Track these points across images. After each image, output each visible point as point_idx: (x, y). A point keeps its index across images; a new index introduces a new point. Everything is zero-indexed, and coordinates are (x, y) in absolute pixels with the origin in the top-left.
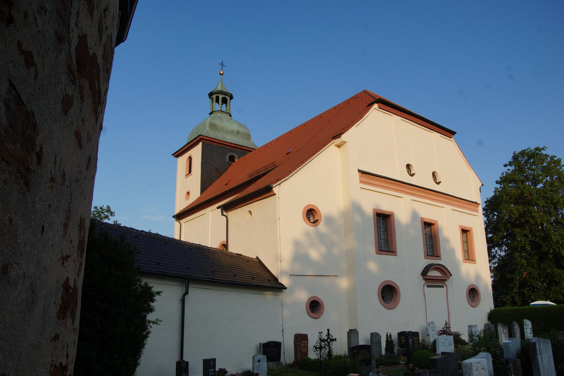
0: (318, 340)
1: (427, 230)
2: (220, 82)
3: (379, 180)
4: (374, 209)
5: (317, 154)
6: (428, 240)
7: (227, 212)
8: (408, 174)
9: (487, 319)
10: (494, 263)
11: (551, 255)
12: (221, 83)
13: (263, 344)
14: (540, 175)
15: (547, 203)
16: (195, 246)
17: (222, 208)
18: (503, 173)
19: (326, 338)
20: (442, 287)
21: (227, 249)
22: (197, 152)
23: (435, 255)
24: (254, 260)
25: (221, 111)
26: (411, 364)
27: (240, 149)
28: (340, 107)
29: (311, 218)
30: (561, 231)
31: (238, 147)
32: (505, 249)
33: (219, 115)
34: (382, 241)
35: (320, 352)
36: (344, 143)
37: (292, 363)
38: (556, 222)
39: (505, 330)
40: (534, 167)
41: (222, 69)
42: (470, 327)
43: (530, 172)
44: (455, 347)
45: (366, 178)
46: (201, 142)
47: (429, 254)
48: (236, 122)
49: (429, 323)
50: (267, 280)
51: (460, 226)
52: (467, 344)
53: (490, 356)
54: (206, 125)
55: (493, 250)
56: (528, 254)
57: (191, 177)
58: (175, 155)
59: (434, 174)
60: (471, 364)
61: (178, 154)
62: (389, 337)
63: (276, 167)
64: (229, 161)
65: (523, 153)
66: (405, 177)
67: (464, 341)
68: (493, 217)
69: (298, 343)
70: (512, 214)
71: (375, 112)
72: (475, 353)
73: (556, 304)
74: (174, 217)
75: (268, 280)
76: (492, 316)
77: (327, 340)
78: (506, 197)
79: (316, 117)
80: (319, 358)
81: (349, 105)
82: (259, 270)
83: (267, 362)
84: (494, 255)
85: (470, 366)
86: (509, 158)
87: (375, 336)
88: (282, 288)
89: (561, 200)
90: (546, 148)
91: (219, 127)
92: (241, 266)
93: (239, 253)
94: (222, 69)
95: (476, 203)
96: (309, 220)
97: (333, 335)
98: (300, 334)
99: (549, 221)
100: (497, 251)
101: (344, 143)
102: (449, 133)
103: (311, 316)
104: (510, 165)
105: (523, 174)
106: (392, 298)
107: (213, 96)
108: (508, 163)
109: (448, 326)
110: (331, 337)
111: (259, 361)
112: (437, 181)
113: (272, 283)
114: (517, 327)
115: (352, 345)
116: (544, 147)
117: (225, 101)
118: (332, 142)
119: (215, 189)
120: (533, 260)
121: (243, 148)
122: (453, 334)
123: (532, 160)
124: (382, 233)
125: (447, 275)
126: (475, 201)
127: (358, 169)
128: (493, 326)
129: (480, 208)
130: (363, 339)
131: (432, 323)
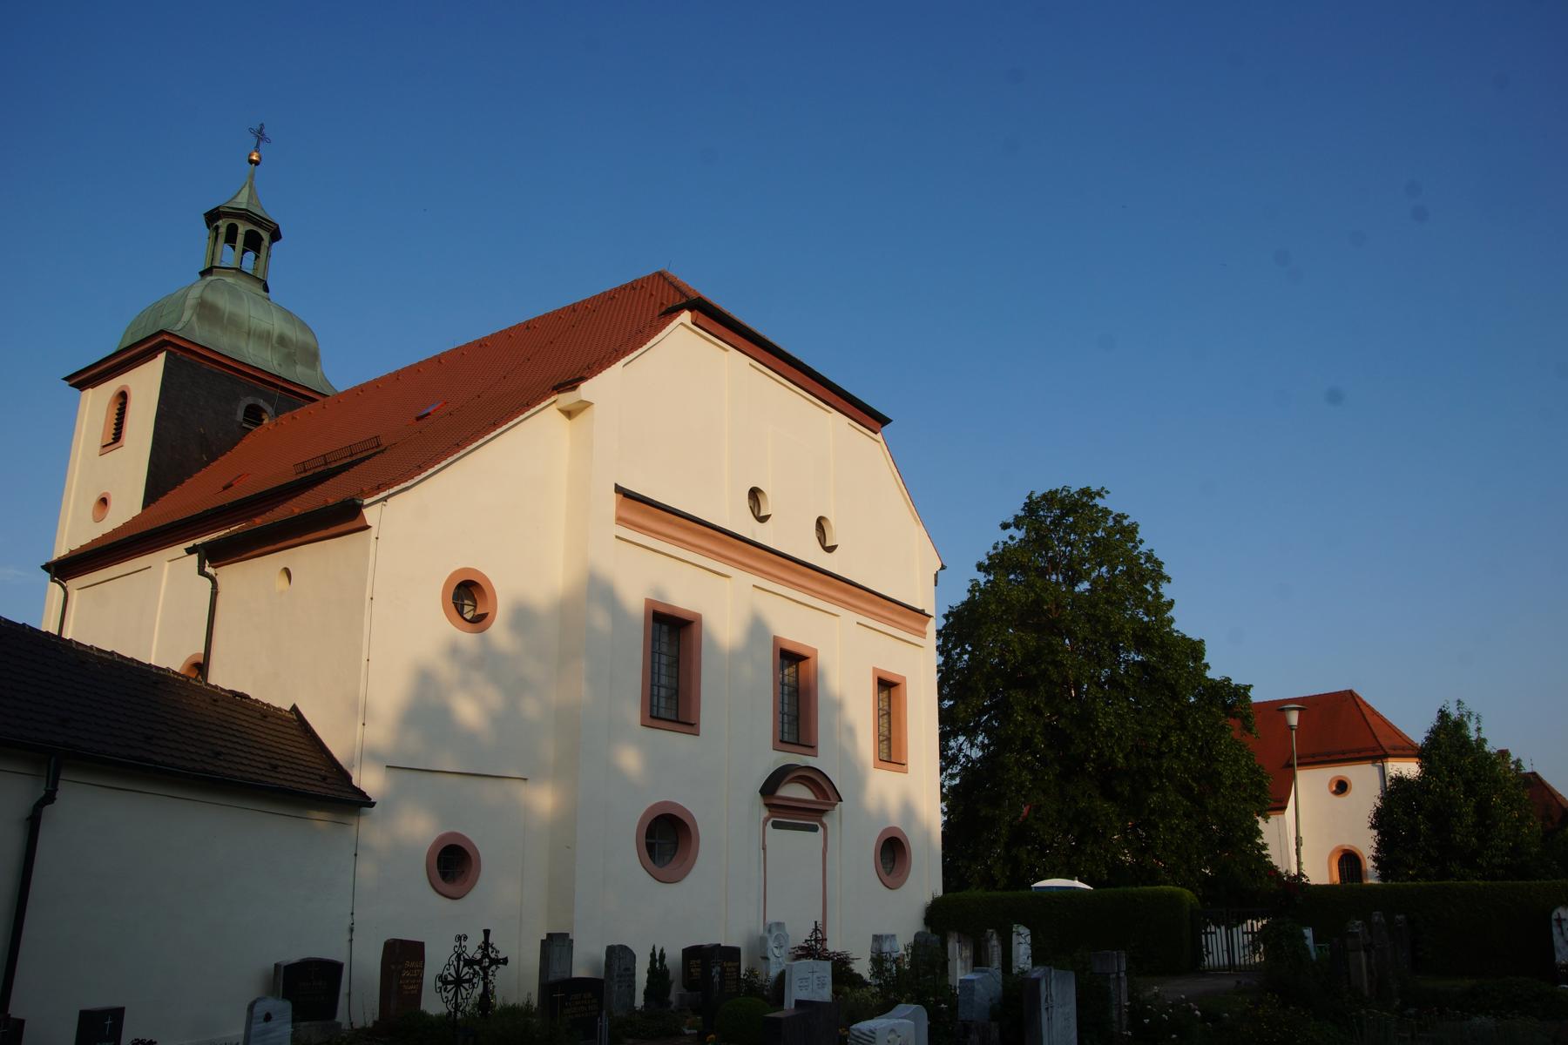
0: (453, 958)
1: (786, 672)
2: (247, 185)
3: (670, 523)
4: (646, 599)
5: (505, 427)
6: (786, 701)
7: (215, 567)
8: (751, 515)
9: (923, 922)
10: (952, 777)
11: (1092, 764)
12: (250, 187)
13: (285, 967)
14: (1087, 560)
15: (1095, 632)
16: (98, 657)
17: (203, 552)
18: (998, 543)
19: (478, 956)
20: (814, 829)
21: (205, 676)
22: (146, 382)
23: (683, 720)
24: (284, 716)
25: (239, 270)
26: (712, 1036)
27: (283, 389)
28: (587, 307)
29: (467, 609)
30: (1120, 706)
31: (276, 382)
32: (982, 742)
33: (230, 280)
34: (663, 692)
35: (456, 993)
36: (585, 405)
37: (370, 1024)
38: (1111, 681)
39: (966, 949)
40: (1072, 537)
41: (258, 146)
42: (877, 939)
43: (1063, 548)
44: (833, 992)
45: (636, 514)
46: (165, 353)
47: (786, 739)
48: (281, 309)
49: (770, 925)
50: (318, 777)
51: (874, 669)
52: (865, 984)
53: (924, 1014)
54: (187, 303)
55: (952, 743)
56: (1038, 760)
57: (115, 455)
58: (73, 382)
59: (821, 524)
60: (874, 1033)
61: (85, 379)
62: (657, 959)
63: (382, 451)
64: (244, 419)
65: (1052, 499)
66: (739, 521)
67: (859, 976)
68: (960, 656)
69: (393, 967)
70: (1009, 651)
71: (681, 335)
72: (884, 1008)
73: (1088, 887)
74: (47, 567)
75: (320, 776)
76: (935, 914)
77: (479, 962)
78: (996, 606)
79: (515, 327)
80: (450, 1012)
81: (613, 306)
82: (296, 744)
83: (294, 1020)
84: (953, 754)
85: (871, 1037)
86: (1016, 508)
87: (619, 956)
88: (358, 802)
89: (1127, 626)
90: (1107, 492)
91: (226, 315)
92: (240, 728)
93: (239, 690)
94: (257, 149)
95: (922, 612)
96: (461, 613)
97: (498, 949)
98: (401, 940)
99: (1095, 679)
100: (961, 745)
101: (585, 405)
102: (871, 418)
103: (439, 889)
104: (1017, 527)
105: (1047, 553)
106: (675, 852)
107: (221, 221)
108: (1011, 520)
109: (820, 935)
110: (492, 952)
111: (268, 1018)
112: (828, 545)
113: (331, 787)
114: (995, 943)
115: (551, 978)
116: (1103, 488)
117: (253, 243)
118: (553, 399)
119: (185, 500)
120: (1047, 774)
121: (292, 388)
122: (832, 959)
123: (1071, 519)
124: (663, 671)
125: (829, 800)
126: (920, 608)
127: (616, 485)
128: (936, 938)
129: (932, 627)
130: (586, 960)
131: (779, 925)
